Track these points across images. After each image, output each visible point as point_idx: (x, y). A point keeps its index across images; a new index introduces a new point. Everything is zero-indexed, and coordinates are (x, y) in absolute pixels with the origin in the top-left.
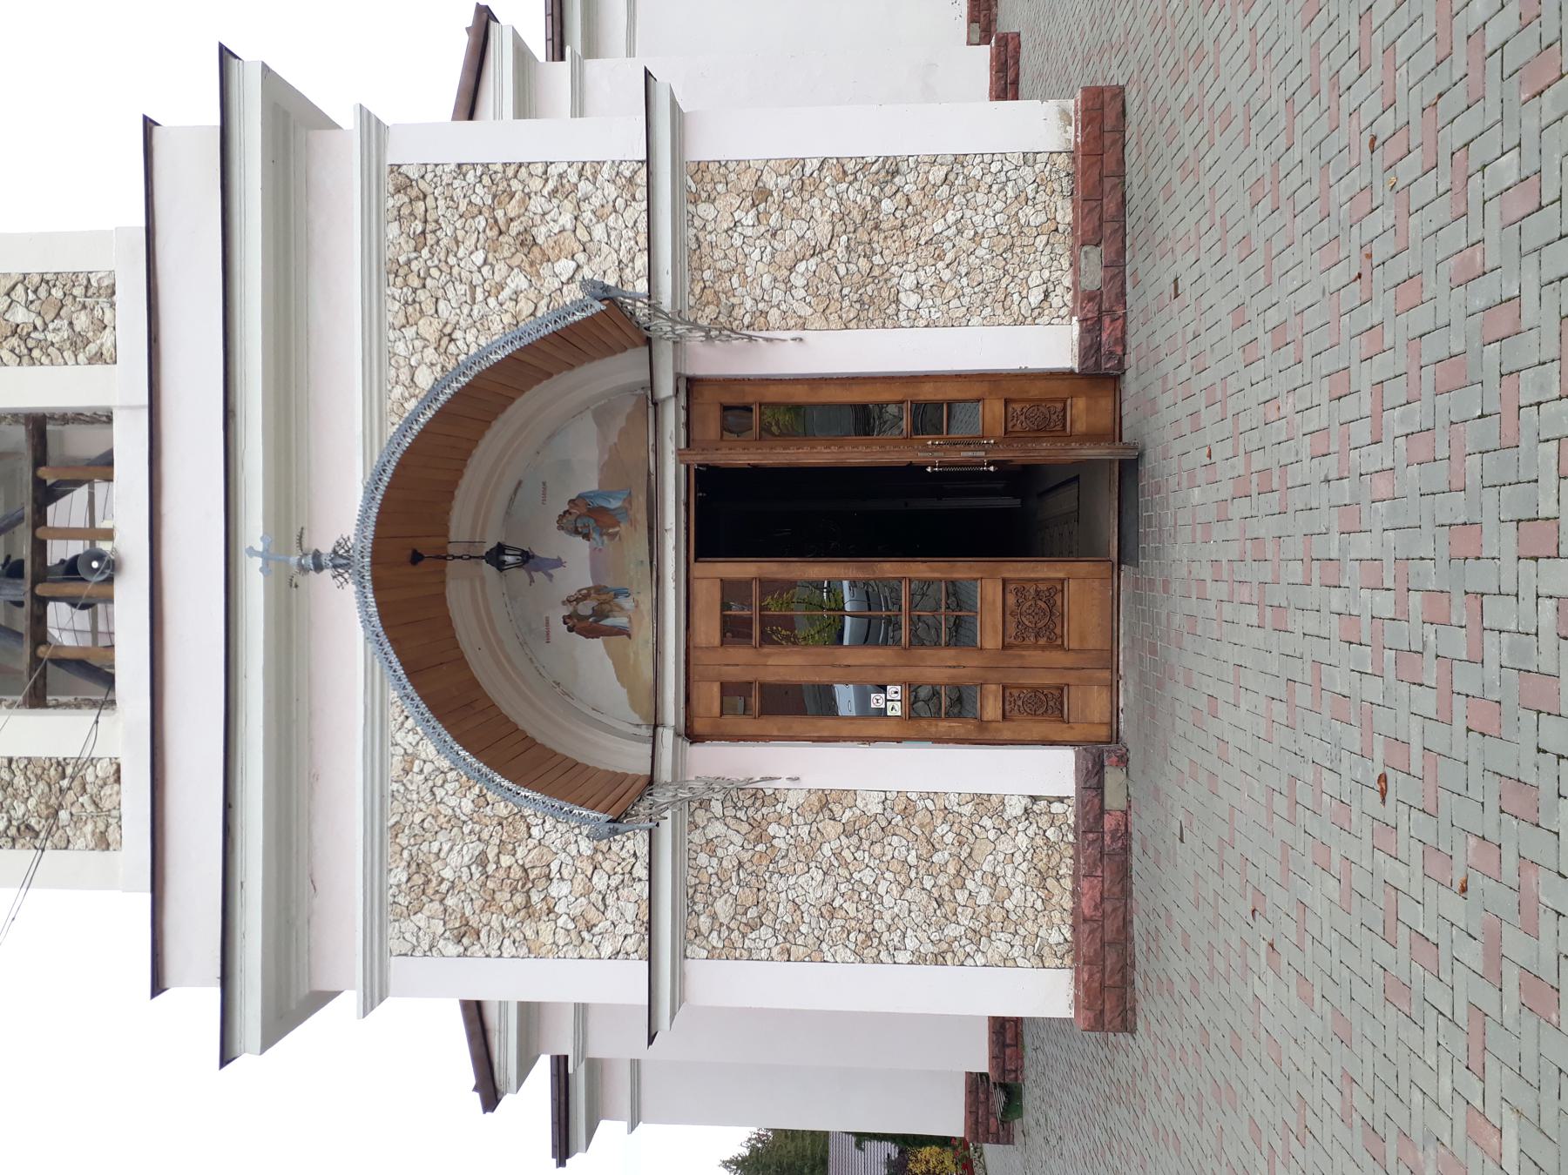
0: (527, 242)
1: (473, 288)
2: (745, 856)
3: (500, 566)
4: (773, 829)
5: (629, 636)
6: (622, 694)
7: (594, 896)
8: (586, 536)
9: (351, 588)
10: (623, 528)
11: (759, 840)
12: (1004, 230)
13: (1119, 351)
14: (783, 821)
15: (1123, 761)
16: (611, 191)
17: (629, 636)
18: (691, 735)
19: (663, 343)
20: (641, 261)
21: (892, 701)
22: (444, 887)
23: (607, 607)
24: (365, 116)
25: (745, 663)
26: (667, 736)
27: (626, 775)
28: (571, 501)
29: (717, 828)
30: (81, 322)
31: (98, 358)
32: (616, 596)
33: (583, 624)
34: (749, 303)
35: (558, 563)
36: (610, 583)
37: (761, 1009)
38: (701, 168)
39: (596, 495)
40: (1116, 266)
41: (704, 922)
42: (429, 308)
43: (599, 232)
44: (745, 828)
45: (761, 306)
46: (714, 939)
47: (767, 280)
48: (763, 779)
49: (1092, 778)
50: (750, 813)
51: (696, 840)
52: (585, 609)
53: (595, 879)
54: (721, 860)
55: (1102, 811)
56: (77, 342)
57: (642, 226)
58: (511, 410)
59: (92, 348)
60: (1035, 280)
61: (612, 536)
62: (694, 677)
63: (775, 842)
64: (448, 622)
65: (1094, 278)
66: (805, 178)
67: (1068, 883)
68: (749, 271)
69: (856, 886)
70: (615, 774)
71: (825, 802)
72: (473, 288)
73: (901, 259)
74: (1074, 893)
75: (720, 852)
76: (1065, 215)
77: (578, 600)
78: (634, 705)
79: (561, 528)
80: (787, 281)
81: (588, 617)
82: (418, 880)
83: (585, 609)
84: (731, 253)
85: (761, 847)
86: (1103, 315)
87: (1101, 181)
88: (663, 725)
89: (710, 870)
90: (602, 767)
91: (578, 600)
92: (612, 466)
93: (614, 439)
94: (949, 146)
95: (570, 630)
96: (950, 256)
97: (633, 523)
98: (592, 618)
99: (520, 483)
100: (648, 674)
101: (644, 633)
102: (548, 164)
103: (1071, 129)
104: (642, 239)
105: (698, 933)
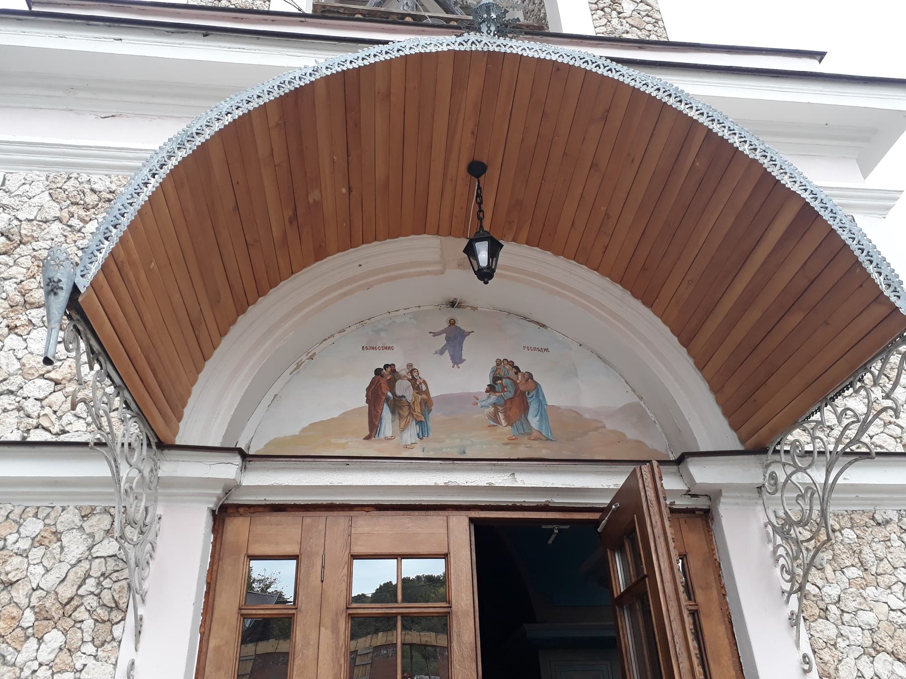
4: (54, 638)
5: (368, 438)
7: (19, 380)
8: (491, 389)
10: (505, 429)
11: (42, 615)
14: (65, 655)
17: (368, 438)
19: (760, 471)
22: (75, 222)
23: (405, 412)
24: (892, 196)
26: (227, 470)
27: (179, 419)
28: (530, 376)
29: (75, 546)
32: (419, 423)
33: (384, 386)
34: (833, 591)
35: (457, 360)
36: (435, 416)
39: (541, 403)
44: (66, 592)
45: (833, 608)
47: (866, 617)
48: (139, 620)
50: (92, 601)
51: (65, 516)
52: (403, 388)
53: (42, 382)
54: (24, 554)
58: (637, 304)
61: (495, 418)
62: (309, 519)
63: (33, 642)
64: (393, 233)
68: (871, 591)
70: (184, 405)
75: (37, 553)
77: (413, 380)
79: (499, 363)
80: (876, 648)
81: (392, 389)
82: (91, 199)
83: (403, 388)
84: (885, 566)
85: (29, 617)
88: (244, 468)
89: (11, 539)
90: (195, 390)
91: (413, 380)
92: (577, 423)
93: (610, 425)
95: (378, 372)
97: (513, 441)
98: (387, 393)
99: (544, 326)
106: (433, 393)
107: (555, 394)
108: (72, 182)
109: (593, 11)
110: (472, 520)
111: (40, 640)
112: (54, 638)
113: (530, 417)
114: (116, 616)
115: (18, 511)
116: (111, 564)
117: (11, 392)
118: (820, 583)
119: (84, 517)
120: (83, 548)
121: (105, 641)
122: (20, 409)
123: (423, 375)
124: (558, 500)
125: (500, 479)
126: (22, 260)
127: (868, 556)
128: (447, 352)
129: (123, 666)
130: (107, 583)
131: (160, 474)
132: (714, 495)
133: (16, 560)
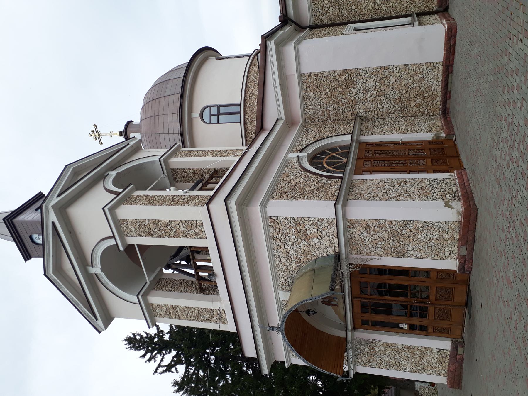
0: (305, 234)
1: (293, 243)
2: (369, 352)
3: (309, 314)
6: (337, 316)
9: (280, 334)
12: (439, 239)
13: (470, 270)
15: (463, 347)
16: (327, 224)
18: (354, 328)
20: (336, 240)
21: (405, 326)
25: (366, 316)
30: (197, 231)
31: (202, 238)
34: (365, 250)
37: (374, 375)
38: (351, 220)
40: (471, 251)
41: (360, 361)
42: (283, 246)
43: (324, 233)
46: (362, 363)
47: (370, 246)
49: (455, 347)
52: (326, 300)
55: (457, 354)
56: (197, 234)
57: (336, 232)
59: (201, 236)
60: (447, 250)
65: (464, 252)
66: (380, 224)
67: (447, 364)
69: (395, 359)
71: (388, 345)
72: (293, 243)
73: (408, 243)
74: (448, 366)
76: (457, 236)
78: (340, 318)
84: (360, 239)
86: (467, 262)
87: (468, 231)
94: (423, 219)
96: (422, 244)
100: (343, 313)
101: (341, 306)
102: (309, 218)
103: (460, 217)
104: (336, 235)
105: (358, 362)
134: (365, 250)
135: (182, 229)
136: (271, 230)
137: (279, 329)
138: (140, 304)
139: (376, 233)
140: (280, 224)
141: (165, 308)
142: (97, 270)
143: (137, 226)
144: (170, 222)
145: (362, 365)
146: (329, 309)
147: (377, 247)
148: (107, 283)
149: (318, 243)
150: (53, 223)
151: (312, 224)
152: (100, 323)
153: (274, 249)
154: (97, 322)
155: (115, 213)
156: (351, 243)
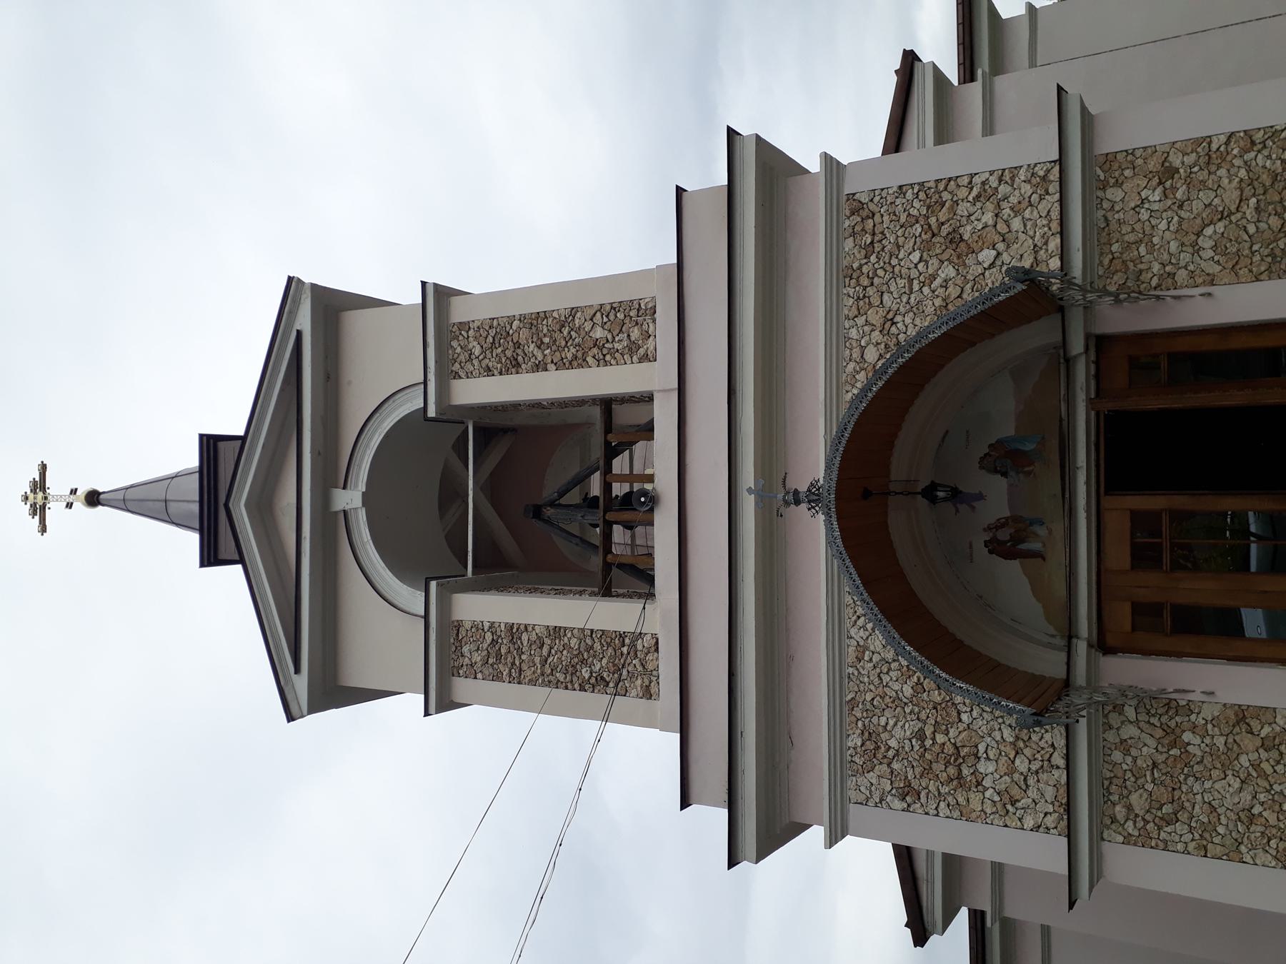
0: (955, 239)
3: (933, 500)
4: (1187, 736)
7: (1016, 776)
8: (1004, 474)
11: (1173, 745)
16: (1027, 189)
18: (1103, 645)
20: (1054, 243)
22: (891, 753)
25: (1151, 585)
26: (1081, 647)
28: (990, 446)
29: (1130, 731)
32: (1031, 524)
34: (1156, 267)
35: (980, 497)
41: (1120, 811)
43: (1016, 224)
44: (1159, 733)
45: (1168, 269)
47: (1174, 246)
48: (1176, 691)
50: (1164, 719)
52: (1004, 535)
53: (1017, 762)
54: (1135, 759)
56: (633, 348)
57: (1055, 214)
61: (1029, 473)
63: (1190, 748)
66: (1208, 153)
68: (1155, 240)
71: (1242, 716)
75: (1134, 752)
77: (997, 528)
79: (981, 468)
81: (1006, 542)
82: (870, 745)
84: (1138, 227)
85: (1174, 752)
89: (1125, 767)
91: (997, 528)
95: (990, 552)
100: (1062, 591)
104: (1055, 226)
105: (1114, 820)
106: (1007, 513)
107: (1007, 429)
108: (856, 759)
109: (606, 364)
110: (1106, 494)
111: (1188, 744)
112: (1187, 736)
113: (1027, 449)
114: (1173, 704)
115: (1106, 766)
116: (1141, 710)
117: (1025, 780)
118: (1150, 275)
119: (1111, 728)
120: (1131, 726)
121: (1189, 709)
122: (1037, 772)
123: (992, 520)
124: (1093, 438)
125: (1081, 477)
126: (924, 784)
127: (1131, 238)
128: (974, 504)
129: (1204, 698)
130: (1153, 712)
131: (1084, 684)
132: (1088, 337)
133: (1139, 762)
134: (1156, 267)
135: (599, 333)
136: (849, 244)
137: (813, 497)
138: (426, 617)
139: (1193, 195)
140: (877, 218)
141: (489, 637)
142: (350, 499)
143: (490, 339)
144: (573, 311)
145: (1128, 840)
146: (1012, 569)
147: (1197, 250)
148: (363, 544)
149: (992, 265)
150: (299, 333)
151: (978, 197)
152: (301, 684)
153: (847, 318)
154: (294, 677)
155: (449, 304)
156: (1106, 249)
